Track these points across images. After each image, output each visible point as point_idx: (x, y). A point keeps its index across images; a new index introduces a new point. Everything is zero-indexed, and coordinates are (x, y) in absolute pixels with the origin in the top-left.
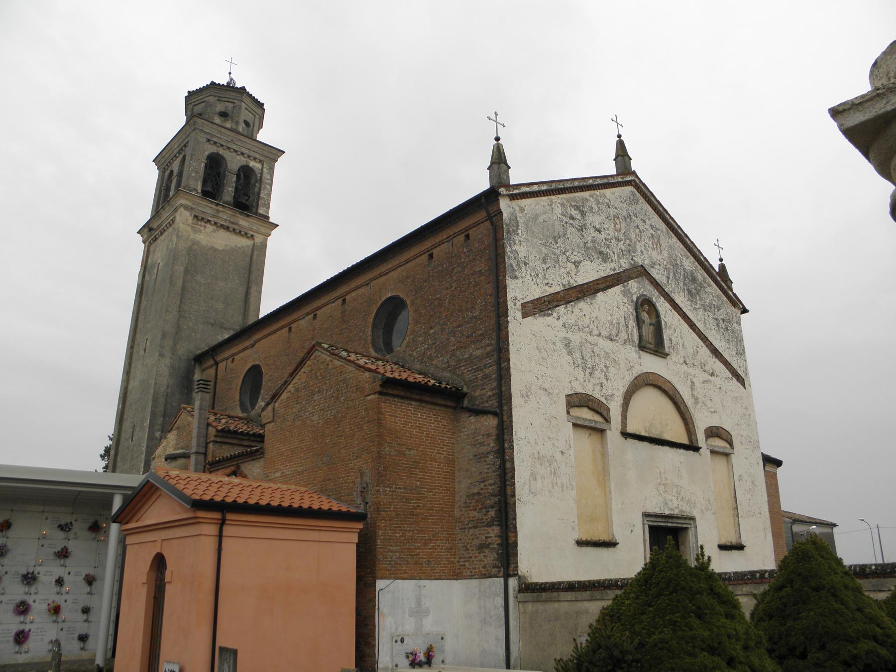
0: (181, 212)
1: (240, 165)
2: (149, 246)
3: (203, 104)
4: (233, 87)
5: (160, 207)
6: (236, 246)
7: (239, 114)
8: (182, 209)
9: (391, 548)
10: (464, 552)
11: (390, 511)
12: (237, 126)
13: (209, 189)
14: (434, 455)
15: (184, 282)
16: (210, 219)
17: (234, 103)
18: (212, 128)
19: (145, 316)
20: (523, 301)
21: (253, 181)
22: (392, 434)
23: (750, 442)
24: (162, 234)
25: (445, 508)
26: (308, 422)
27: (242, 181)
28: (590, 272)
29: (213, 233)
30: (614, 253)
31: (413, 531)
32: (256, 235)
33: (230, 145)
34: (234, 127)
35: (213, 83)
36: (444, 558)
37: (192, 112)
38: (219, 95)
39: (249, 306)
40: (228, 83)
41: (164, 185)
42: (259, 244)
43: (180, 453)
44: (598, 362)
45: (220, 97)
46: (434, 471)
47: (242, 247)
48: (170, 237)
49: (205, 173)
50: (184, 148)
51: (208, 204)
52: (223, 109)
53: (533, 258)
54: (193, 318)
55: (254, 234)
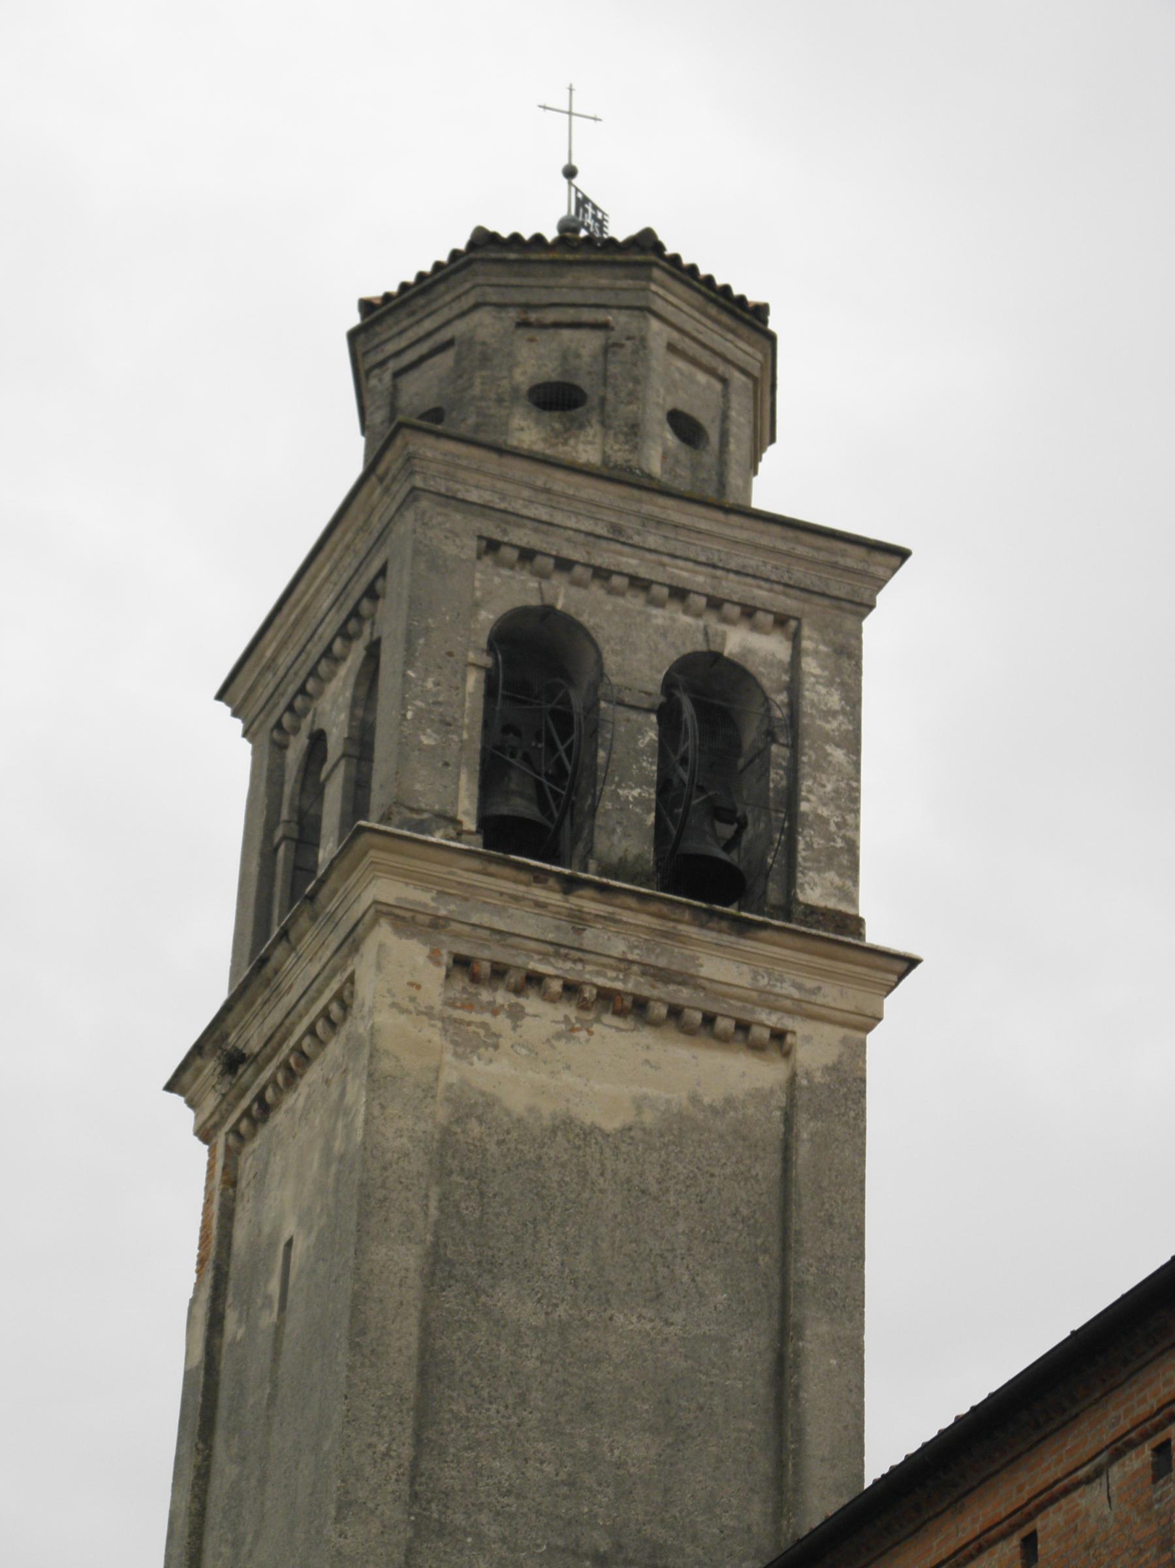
0: (381, 946)
1: (674, 656)
2: (232, 1156)
3: (446, 359)
4: (589, 240)
5: (276, 931)
6: (695, 1099)
7: (636, 381)
8: (383, 932)
12: (635, 448)
13: (520, 806)
15: (426, 1330)
16: (542, 968)
17: (604, 326)
18: (503, 478)
19: (236, 1544)
21: (750, 736)
24: (292, 1076)
27: (689, 744)
29: (561, 1045)
32: (799, 1027)
33: (604, 559)
34: (619, 454)
35: (483, 240)
37: (394, 409)
38: (520, 297)
39: (799, 1433)
40: (567, 228)
41: (285, 814)
42: (818, 1077)
45: (527, 307)
47: (729, 1102)
48: (334, 1093)
49: (486, 725)
50: (366, 606)
51: (521, 889)
52: (550, 371)
54: (492, 1531)
55: (788, 1023)
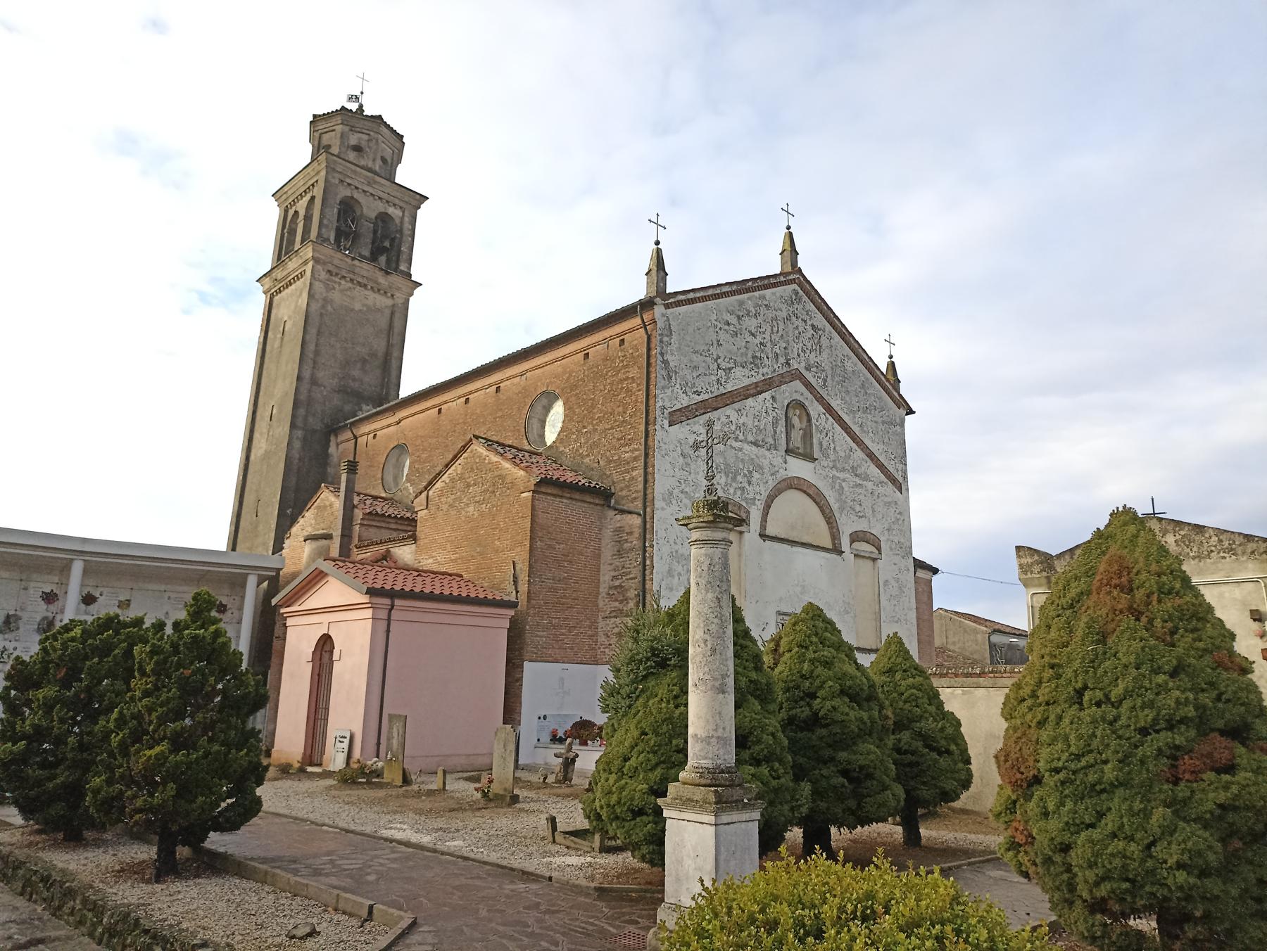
17: (369, 135)
20: (670, 410)
23: (901, 548)
26: (463, 513)
28: (741, 379)
30: (768, 358)
43: (321, 535)
53: (684, 367)
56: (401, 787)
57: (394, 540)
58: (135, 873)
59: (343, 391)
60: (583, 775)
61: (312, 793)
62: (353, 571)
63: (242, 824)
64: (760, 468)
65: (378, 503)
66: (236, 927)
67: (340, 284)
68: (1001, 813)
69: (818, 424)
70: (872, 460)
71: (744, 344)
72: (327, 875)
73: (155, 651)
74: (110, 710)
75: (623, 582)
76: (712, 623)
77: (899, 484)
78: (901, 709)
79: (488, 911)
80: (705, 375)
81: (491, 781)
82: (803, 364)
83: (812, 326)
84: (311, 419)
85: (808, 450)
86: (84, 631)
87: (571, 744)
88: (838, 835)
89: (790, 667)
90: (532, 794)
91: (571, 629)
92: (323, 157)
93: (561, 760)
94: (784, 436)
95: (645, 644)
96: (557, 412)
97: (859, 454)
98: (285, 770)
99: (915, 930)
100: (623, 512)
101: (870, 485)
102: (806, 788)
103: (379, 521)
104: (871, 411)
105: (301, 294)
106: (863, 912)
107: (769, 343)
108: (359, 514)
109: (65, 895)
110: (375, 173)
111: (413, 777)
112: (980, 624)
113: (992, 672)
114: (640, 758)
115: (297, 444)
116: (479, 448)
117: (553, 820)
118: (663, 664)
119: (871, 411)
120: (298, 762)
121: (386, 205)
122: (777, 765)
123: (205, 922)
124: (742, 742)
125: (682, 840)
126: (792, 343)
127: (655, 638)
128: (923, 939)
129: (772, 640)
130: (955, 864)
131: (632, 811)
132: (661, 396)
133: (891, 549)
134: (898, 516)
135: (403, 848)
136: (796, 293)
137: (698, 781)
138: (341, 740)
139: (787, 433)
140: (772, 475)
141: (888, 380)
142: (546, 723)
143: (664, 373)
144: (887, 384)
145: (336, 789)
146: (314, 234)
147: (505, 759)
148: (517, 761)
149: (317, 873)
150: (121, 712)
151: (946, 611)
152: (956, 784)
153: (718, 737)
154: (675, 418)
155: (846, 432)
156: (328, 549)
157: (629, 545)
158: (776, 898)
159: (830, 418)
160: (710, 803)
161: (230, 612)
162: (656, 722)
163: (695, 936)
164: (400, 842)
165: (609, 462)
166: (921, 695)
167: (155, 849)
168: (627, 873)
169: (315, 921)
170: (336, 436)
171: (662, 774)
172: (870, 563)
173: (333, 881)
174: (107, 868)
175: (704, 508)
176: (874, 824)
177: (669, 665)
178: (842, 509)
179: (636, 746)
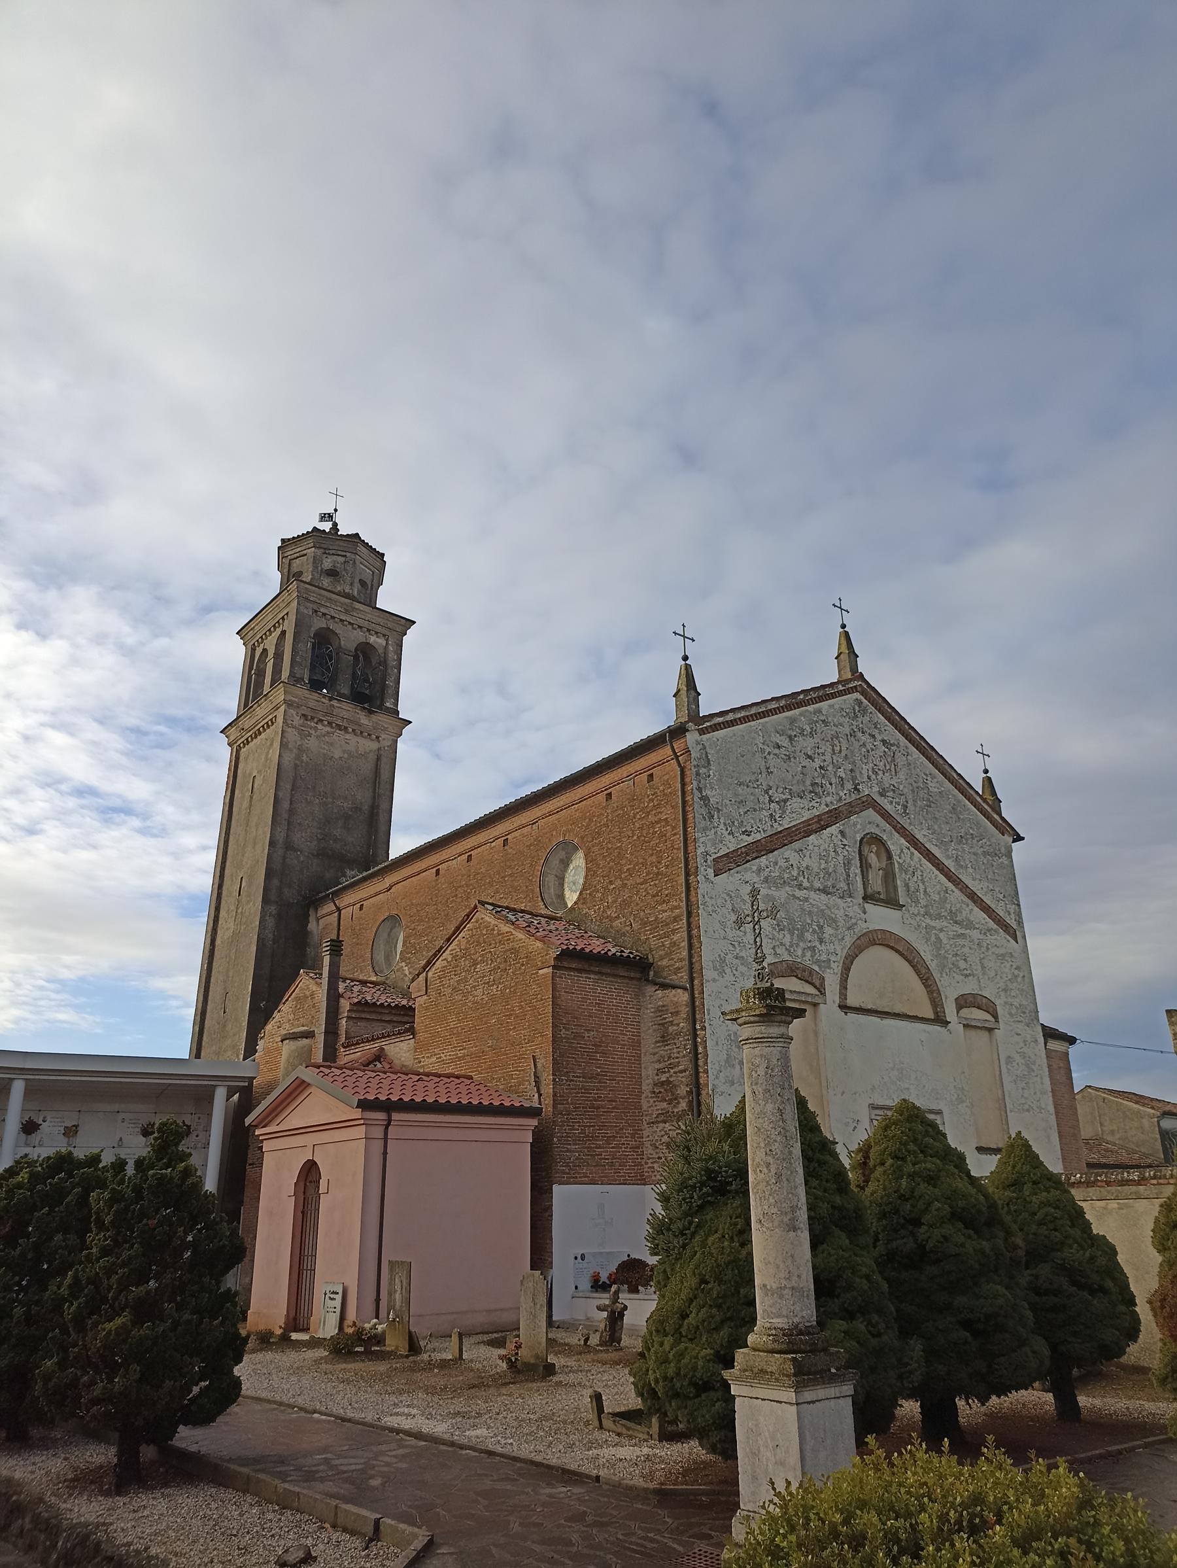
2: (238, 752)
9: (569, 1147)
10: (652, 1152)
11: (568, 1103)
14: (617, 1037)
17: (345, 556)
22: (567, 1013)
23: (1024, 1013)
25: (630, 1099)
28: (800, 812)
30: (831, 784)
31: (594, 1126)
36: (630, 1159)
38: (325, 546)
44: (809, 922)
45: (325, 549)
46: (617, 1055)
53: (728, 802)
56: (407, 1357)
57: (389, 1036)
58: (92, 1482)
59: (323, 854)
60: (633, 1331)
61: (298, 1368)
62: (341, 1079)
63: (219, 1413)
64: (833, 921)
65: (368, 990)
66: (215, 1552)
67: (316, 729)
68: (1167, 1378)
69: (901, 861)
70: (975, 902)
71: (800, 769)
72: (322, 1480)
73: (116, 1197)
74: (62, 1272)
75: (671, 1076)
76: (775, 1141)
77: (1014, 932)
78: (1035, 1234)
79: (520, 1524)
80: (755, 810)
81: (518, 1347)
82: (876, 789)
83: (883, 741)
84: (286, 891)
85: (892, 895)
86: (32, 1175)
87: (617, 1293)
88: (968, 1410)
89: (884, 1185)
90: (571, 1362)
91: (609, 1140)
92: (293, 587)
93: (605, 1314)
94: (859, 879)
95: (698, 1165)
96: (577, 870)
97: (957, 895)
98: (266, 1340)
99: (1033, 1544)
100: (664, 986)
101: (975, 934)
102: (917, 1348)
103: (368, 1012)
104: (967, 840)
105: (272, 744)
106: (970, 1521)
107: (831, 766)
108: (345, 1005)
109: (11, 1512)
110: (353, 598)
111: (422, 1343)
112: (1144, 1105)
113: (1155, 1177)
114: (700, 1315)
115: (271, 922)
116: (485, 916)
117: (597, 1398)
118: (722, 1190)
119: (967, 840)
120: (280, 1327)
121: (367, 634)
122: (875, 1318)
123: (178, 1547)
124: (825, 1286)
125: (757, 1425)
126: (859, 763)
127: (711, 1158)
128: (1043, 1555)
129: (860, 1150)
130: (1126, 1446)
131: (695, 1385)
132: (702, 840)
133: (1011, 1015)
134: (1016, 972)
135: (412, 1441)
136: (860, 703)
137: (770, 1346)
138: (332, 1296)
139: (863, 875)
140: (849, 929)
141: (985, 800)
142: (585, 1264)
143: (704, 811)
144: (986, 807)
145: (326, 1363)
146: (285, 674)
147: (535, 1316)
148: (550, 1316)
149: (309, 1477)
150: (75, 1277)
151: (1097, 1089)
152: (1118, 1333)
153: (793, 1288)
154: (720, 865)
155: (938, 869)
156: (310, 1051)
157: (675, 1028)
158: (863, 1505)
159: (916, 852)
160: (788, 1376)
161: (195, 1133)
162: (718, 1266)
163: (767, 1556)
164: (408, 1433)
165: (644, 924)
166: (1058, 1214)
167: (113, 1450)
168: (692, 1470)
169: (309, 1542)
170: (316, 910)
171: (731, 1335)
172: (985, 1034)
173: (330, 1487)
174: (58, 1477)
175: (754, 998)
176: (1013, 1392)
177: (729, 1192)
178: (942, 967)
179: (696, 1298)
